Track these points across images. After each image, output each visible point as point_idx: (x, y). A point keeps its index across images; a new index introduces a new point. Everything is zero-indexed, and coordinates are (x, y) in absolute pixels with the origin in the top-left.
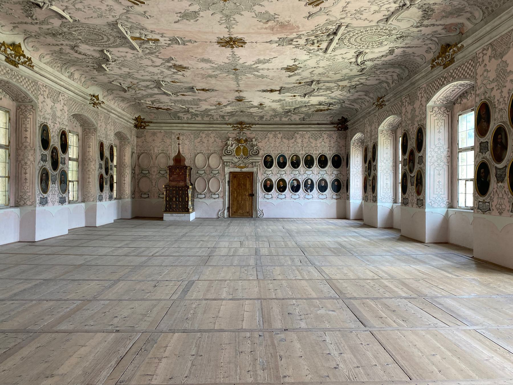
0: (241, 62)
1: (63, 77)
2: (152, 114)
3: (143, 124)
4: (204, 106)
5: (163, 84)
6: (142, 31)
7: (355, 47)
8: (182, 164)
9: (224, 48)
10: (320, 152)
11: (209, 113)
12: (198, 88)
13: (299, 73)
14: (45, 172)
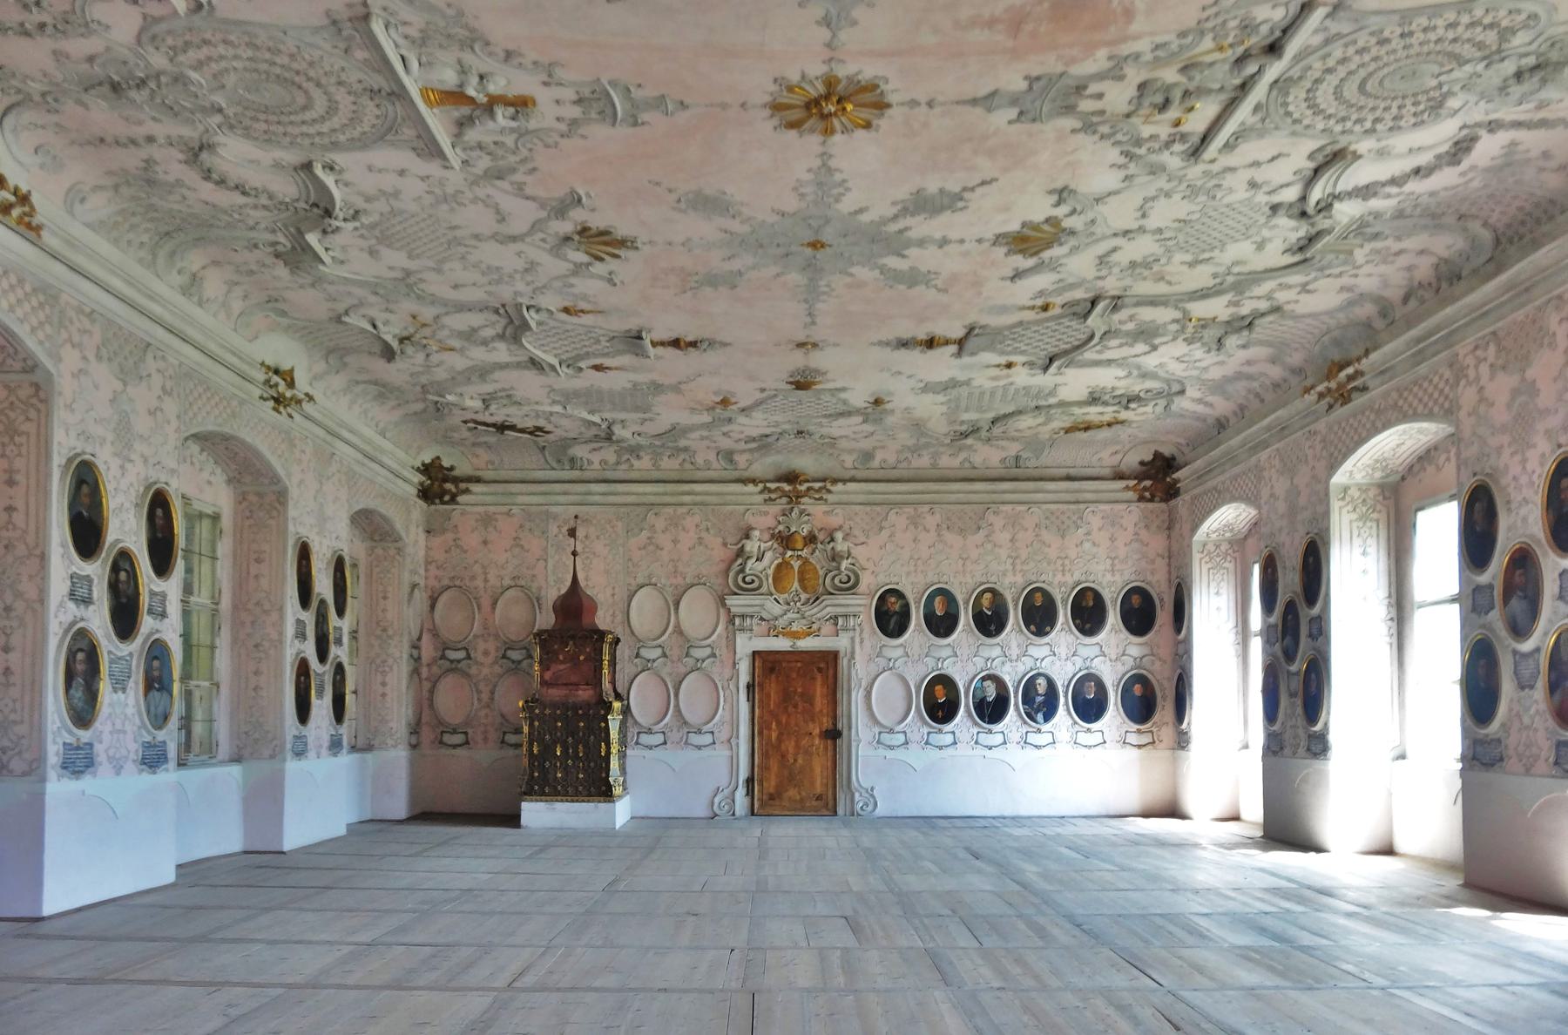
0: (847, 205)
1: (160, 287)
2: (480, 451)
3: (448, 486)
4: (668, 413)
5: (532, 318)
6: (468, 57)
7: (1320, 126)
8: (585, 621)
9: (793, 133)
10: (1077, 576)
11: (683, 443)
12: (657, 337)
13: (1058, 258)
14: (84, 644)
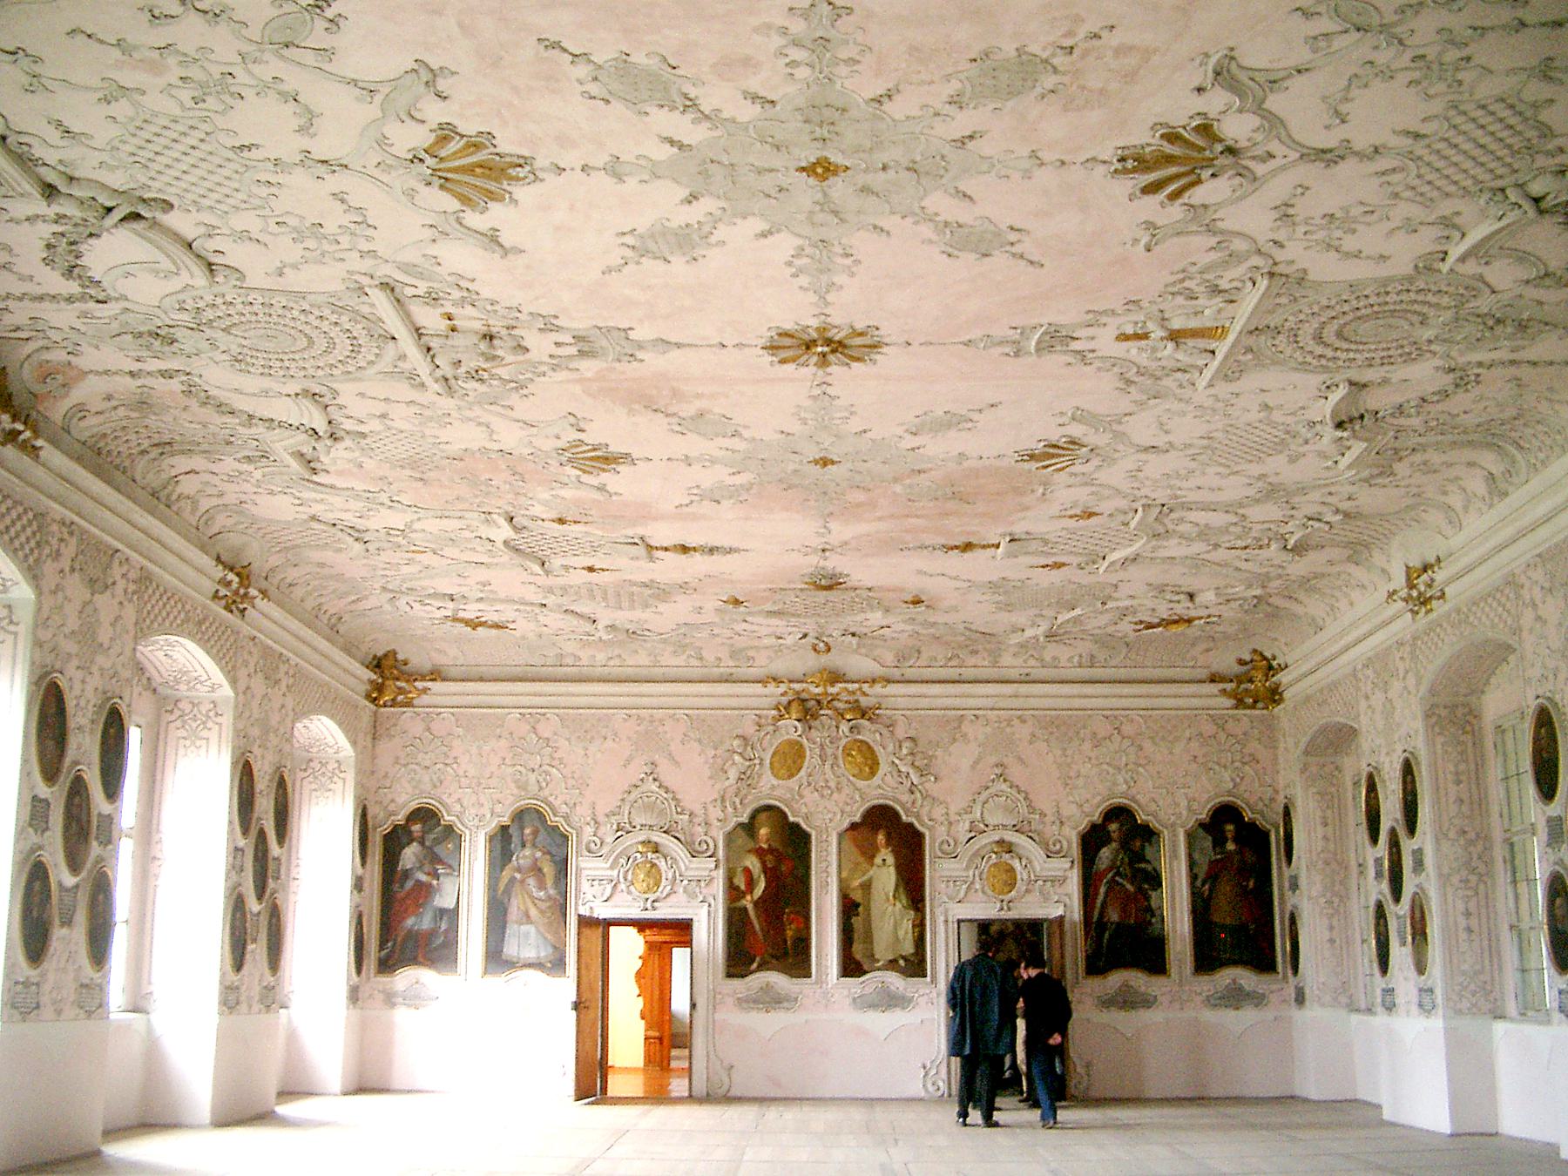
0: (784, 244)
